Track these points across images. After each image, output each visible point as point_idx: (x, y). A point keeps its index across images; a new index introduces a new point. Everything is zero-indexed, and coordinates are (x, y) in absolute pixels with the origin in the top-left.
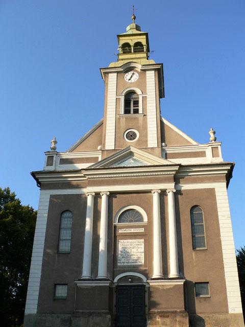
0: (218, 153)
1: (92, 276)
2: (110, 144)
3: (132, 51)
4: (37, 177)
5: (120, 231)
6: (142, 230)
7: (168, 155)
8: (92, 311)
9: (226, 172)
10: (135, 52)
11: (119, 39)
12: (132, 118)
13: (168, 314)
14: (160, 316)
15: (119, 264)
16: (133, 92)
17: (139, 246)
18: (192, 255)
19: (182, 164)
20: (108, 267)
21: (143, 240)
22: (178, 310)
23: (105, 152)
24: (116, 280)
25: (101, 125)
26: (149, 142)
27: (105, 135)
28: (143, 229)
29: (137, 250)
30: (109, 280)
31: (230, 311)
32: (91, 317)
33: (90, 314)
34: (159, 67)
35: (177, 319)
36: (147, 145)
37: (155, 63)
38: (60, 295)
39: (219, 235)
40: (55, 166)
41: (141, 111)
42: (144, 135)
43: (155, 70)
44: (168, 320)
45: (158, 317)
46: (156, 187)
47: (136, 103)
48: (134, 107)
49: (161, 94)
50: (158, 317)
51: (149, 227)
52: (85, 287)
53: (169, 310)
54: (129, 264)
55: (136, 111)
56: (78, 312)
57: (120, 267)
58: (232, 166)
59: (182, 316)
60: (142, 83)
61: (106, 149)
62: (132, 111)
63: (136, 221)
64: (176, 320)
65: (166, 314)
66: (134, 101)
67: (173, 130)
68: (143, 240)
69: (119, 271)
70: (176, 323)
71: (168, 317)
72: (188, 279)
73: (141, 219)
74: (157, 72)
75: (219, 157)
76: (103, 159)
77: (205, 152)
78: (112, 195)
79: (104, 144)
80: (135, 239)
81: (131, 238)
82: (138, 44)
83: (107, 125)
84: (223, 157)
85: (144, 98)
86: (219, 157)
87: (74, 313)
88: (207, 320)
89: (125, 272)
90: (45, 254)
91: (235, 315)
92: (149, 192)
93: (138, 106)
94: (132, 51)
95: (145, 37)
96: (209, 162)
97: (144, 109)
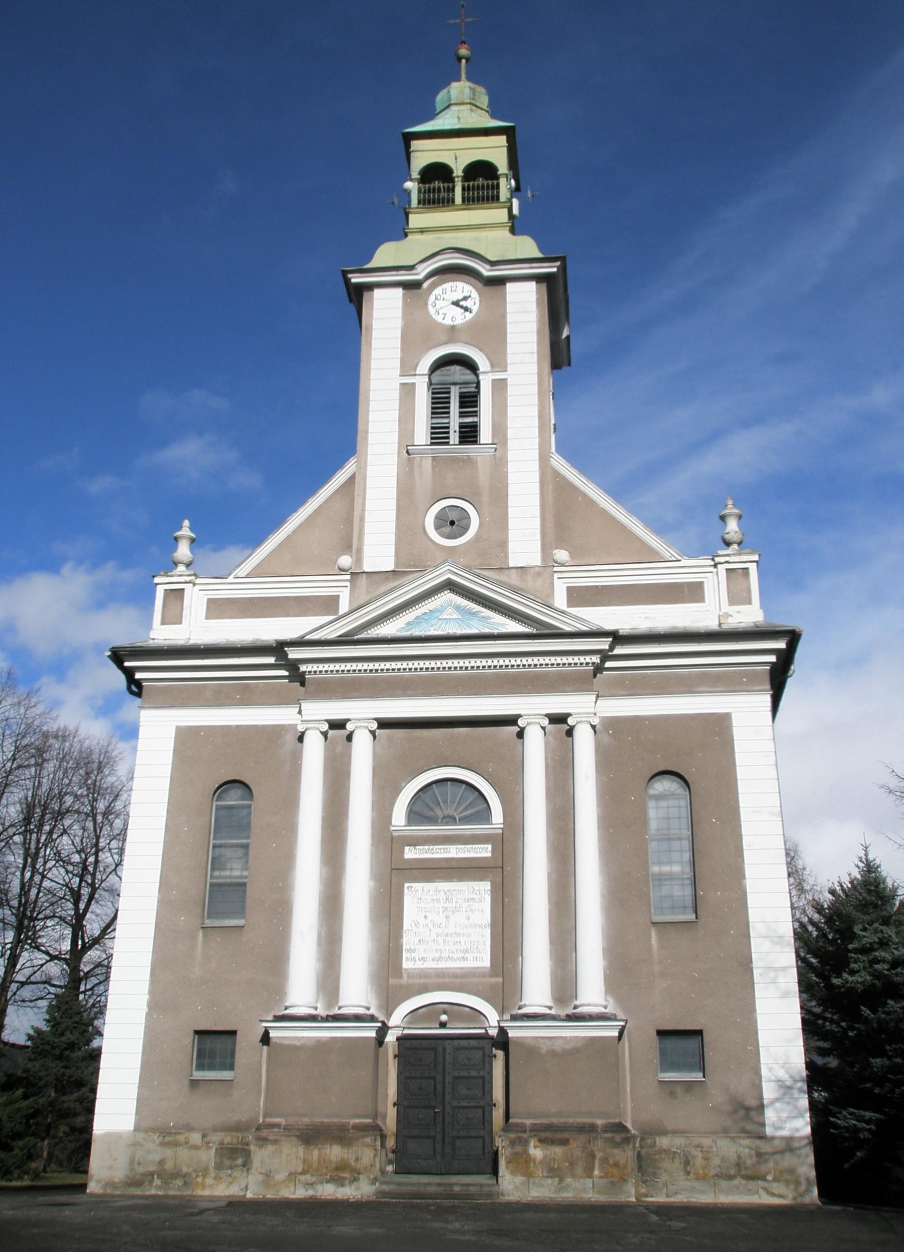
0: (749, 591)
1: (319, 1005)
3: (458, 199)
4: (126, 664)
6: (484, 851)
7: (490, 1170)
9: (773, 658)
10: (469, 201)
11: (407, 146)
12: (454, 460)
13: (565, 1135)
14: (540, 1141)
15: (406, 965)
19: (621, 632)
20: (318, 985)
22: (599, 1122)
23: (363, 581)
24: (397, 1018)
26: (512, 547)
27: (362, 519)
28: (489, 847)
29: (468, 918)
30: (372, 1019)
31: (489, 883)
34: (551, 268)
36: (506, 557)
37: (540, 255)
38: (419, 965)
39: (739, 873)
41: (485, 434)
47: (470, 401)
48: (462, 414)
49: (553, 398)
52: (298, 1043)
53: (571, 1120)
55: (469, 434)
57: (412, 974)
58: (793, 637)
59: (611, 1141)
61: (366, 569)
62: (454, 438)
63: (465, 820)
65: (559, 1136)
66: (462, 396)
67: (592, 503)
69: (408, 986)
72: (708, 1083)
73: (485, 815)
74: (544, 287)
75: (749, 602)
76: (355, 606)
77: (700, 585)
79: (360, 551)
80: (461, 880)
81: (448, 878)
84: (763, 606)
85: (500, 386)
86: (749, 602)
87: (258, 1129)
89: (424, 989)
91: (789, 1145)
93: (475, 414)
94: (458, 199)
95: (502, 140)
96: (711, 623)
97: (500, 430)
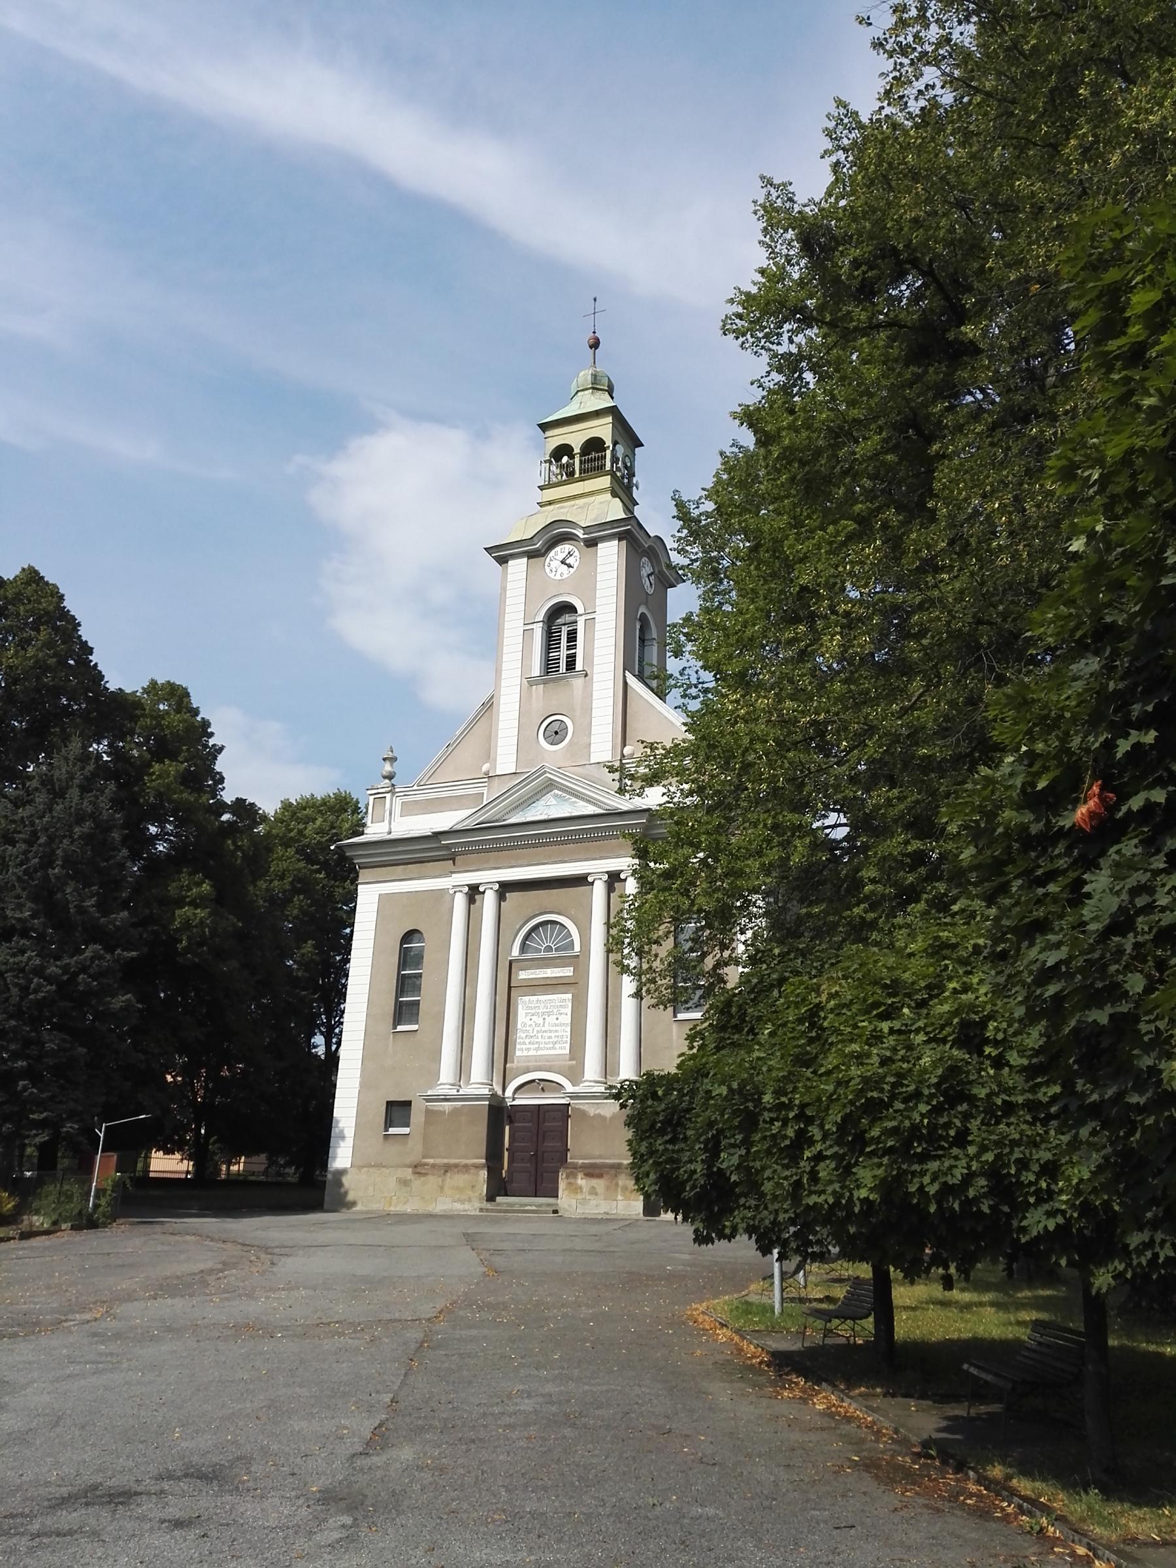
2: (506, 762)
5: (523, 975)
6: (568, 972)
8: (453, 1161)
16: (569, 608)
17: (562, 1011)
18: (671, 1031)
21: (570, 996)
25: (489, 706)
32: (449, 1174)
33: (447, 1168)
35: (620, 1183)
40: (390, 823)
42: (586, 729)
43: (620, 537)
44: (599, 1184)
45: (580, 1175)
46: (596, 867)
50: (580, 1175)
51: (580, 962)
54: (540, 1053)
56: (427, 1164)
60: (589, 581)
64: (617, 1185)
65: (597, 1171)
68: (570, 996)
70: (616, 1190)
71: (600, 1176)
78: (505, 888)
79: (495, 760)
82: (594, 445)
83: (502, 708)
88: (984, 1330)
89: (528, 1070)
90: (333, 1034)
92: (581, 881)
97: (589, 658)
